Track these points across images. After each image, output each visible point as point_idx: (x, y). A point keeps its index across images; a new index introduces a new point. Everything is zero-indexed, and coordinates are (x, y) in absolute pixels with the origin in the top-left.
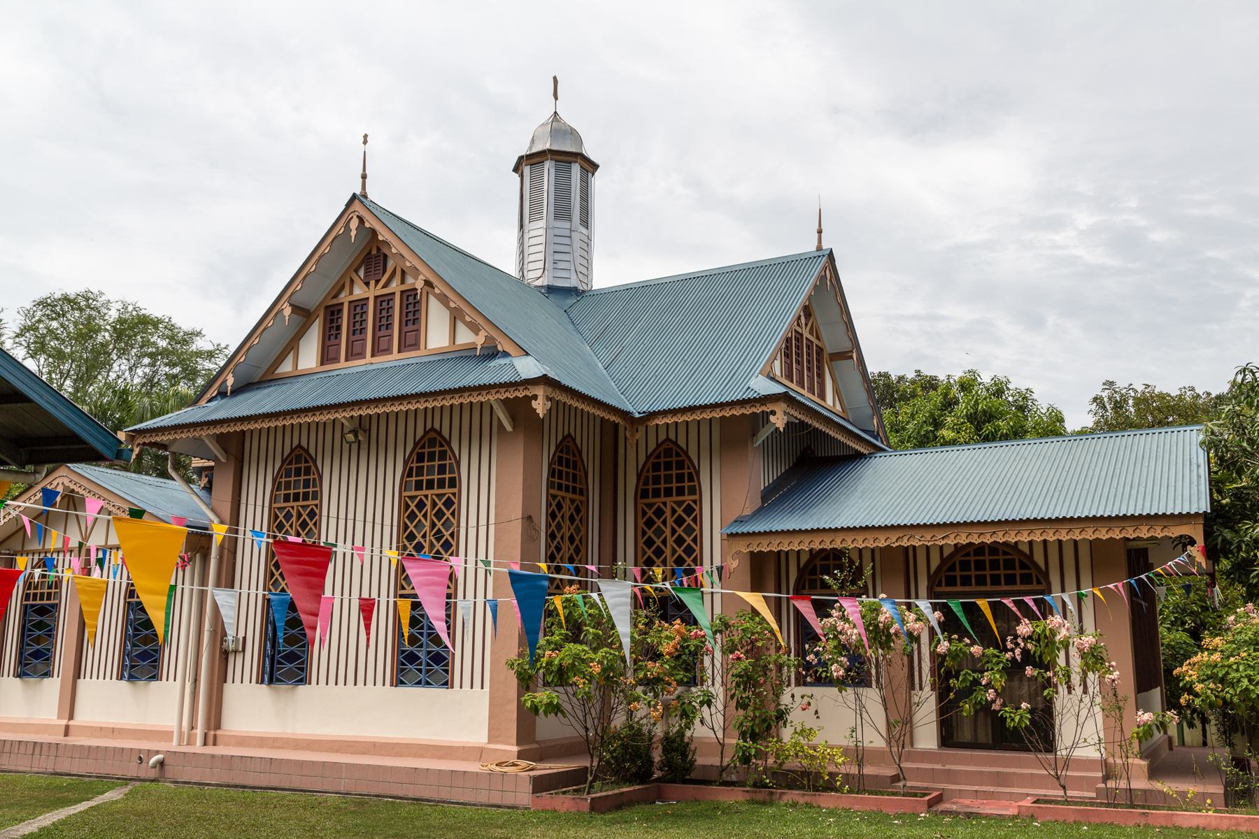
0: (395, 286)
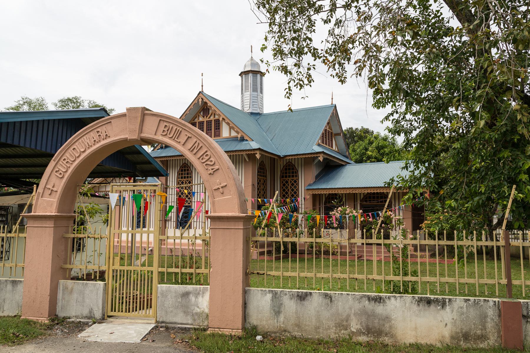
0: (212, 118)
